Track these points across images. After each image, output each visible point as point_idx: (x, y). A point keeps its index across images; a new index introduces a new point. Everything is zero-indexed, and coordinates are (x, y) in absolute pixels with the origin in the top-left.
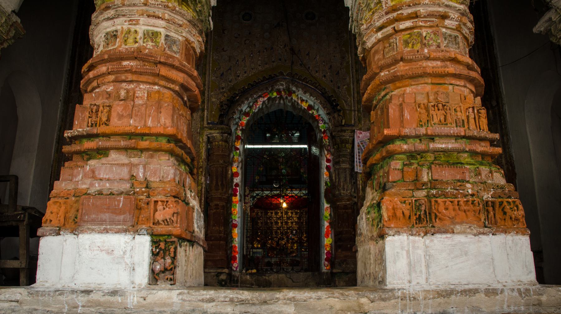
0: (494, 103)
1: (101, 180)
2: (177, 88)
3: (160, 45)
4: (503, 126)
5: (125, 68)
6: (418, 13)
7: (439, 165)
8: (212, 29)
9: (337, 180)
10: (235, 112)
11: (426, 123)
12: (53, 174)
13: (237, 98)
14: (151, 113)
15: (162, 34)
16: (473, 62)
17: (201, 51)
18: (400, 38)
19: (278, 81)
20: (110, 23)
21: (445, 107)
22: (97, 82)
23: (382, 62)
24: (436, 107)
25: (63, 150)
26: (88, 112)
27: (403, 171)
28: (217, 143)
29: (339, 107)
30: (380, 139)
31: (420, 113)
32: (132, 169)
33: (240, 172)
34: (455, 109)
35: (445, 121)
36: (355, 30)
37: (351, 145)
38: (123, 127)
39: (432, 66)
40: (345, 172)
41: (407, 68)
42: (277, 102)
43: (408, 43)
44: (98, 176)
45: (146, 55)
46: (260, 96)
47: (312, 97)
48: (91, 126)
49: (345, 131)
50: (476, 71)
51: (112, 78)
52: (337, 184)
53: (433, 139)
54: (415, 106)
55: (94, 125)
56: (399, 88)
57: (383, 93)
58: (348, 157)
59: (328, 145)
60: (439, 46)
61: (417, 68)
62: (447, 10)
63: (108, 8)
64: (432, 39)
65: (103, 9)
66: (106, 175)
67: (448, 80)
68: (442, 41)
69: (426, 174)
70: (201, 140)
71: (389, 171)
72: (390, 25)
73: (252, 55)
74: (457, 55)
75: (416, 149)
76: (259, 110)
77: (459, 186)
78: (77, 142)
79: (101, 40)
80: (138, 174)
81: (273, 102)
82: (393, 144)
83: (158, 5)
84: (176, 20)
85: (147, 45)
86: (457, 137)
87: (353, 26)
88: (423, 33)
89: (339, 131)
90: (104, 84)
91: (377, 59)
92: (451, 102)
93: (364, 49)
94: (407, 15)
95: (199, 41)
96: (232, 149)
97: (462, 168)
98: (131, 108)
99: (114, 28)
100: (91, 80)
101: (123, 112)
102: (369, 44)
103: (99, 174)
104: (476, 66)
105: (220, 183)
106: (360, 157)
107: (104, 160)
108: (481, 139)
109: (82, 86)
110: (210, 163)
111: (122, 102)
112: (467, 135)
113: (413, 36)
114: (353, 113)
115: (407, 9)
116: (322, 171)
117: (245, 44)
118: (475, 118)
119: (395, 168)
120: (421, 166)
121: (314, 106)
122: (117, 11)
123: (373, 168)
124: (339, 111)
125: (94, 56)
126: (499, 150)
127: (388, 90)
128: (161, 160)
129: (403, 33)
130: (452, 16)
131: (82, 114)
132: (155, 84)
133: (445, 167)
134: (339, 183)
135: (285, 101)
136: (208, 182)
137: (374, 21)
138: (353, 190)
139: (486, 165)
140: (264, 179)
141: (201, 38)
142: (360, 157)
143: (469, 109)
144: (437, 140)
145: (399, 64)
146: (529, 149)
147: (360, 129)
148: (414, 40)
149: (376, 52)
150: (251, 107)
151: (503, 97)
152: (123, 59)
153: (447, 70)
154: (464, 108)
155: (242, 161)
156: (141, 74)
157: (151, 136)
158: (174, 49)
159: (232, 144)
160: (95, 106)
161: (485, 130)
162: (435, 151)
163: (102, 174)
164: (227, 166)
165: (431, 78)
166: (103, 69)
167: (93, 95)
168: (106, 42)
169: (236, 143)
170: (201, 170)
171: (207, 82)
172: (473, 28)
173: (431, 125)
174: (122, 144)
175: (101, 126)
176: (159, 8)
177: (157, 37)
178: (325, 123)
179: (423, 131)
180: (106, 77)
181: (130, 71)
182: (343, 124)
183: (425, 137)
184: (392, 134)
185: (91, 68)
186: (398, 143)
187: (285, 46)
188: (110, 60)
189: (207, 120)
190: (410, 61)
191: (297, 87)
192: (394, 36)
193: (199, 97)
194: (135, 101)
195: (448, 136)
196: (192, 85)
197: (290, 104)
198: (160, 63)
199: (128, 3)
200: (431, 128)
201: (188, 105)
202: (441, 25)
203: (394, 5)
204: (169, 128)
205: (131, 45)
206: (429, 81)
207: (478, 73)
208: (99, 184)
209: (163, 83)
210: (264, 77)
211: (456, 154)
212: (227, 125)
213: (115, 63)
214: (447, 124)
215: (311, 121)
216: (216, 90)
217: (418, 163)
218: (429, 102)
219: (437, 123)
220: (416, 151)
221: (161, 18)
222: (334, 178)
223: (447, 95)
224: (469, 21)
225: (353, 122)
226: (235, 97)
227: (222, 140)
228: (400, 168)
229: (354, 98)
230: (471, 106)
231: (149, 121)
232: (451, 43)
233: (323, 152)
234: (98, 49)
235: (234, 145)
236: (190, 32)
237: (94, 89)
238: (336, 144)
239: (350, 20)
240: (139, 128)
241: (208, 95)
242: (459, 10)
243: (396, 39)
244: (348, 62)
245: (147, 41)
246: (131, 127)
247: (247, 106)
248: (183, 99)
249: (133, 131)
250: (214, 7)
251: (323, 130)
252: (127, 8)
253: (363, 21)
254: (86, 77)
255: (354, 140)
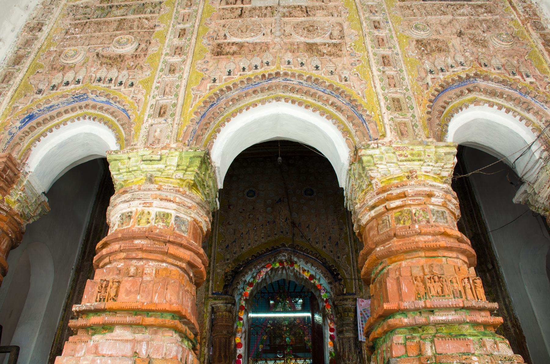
0: (490, 266)
1: (103, 356)
2: (184, 265)
3: (170, 225)
4: (503, 288)
5: (136, 246)
6: (406, 193)
7: (442, 337)
8: (218, 209)
9: (342, 350)
10: (239, 283)
11: (424, 296)
12: (55, 342)
13: (241, 269)
14: (157, 289)
15: (173, 215)
16: (462, 234)
17: (208, 230)
18: (391, 215)
19: (280, 252)
20: (126, 205)
21: (441, 279)
22: (109, 259)
23: (377, 238)
24: (432, 280)
25: (69, 324)
26: (98, 287)
27: (405, 346)
28: (221, 313)
29: (339, 276)
30: (381, 313)
31: (417, 286)
32: (135, 346)
33: (243, 342)
34: (450, 281)
35: (442, 293)
36: (350, 207)
37: (354, 314)
38: (130, 303)
39: (424, 240)
40: (349, 342)
41: (401, 243)
42: (280, 272)
43: (400, 220)
44: (101, 352)
45: (157, 234)
46: (264, 267)
47: (313, 267)
48: (100, 301)
49: (346, 300)
50: (466, 243)
51: (123, 255)
52: (341, 354)
53: (432, 311)
54: (412, 279)
55: (102, 300)
56: (395, 262)
57: (380, 267)
58: (352, 326)
59: (331, 314)
60: (428, 222)
61: (411, 243)
62: (432, 189)
63: (125, 192)
64: (421, 215)
65: (121, 193)
66: (109, 351)
67: (441, 253)
68: (430, 217)
69: (429, 347)
70: (205, 310)
71: (391, 346)
72: (381, 204)
73: (255, 229)
74: (446, 229)
75: (417, 323)
76: (262, 280)
77: (464, 360)
78: (84, 316)
79: (117, 220)
80: (141, 350)
81: (275, 272)
82: (394, 318)
83: (170, 190)
84: (186, 203)
85: (158, 225)
86: (457, 309)
87: (348, 204)
88: (412, 210)
89: (341, 300)
90: (115, 261)
91: (372, 236)
92: (445, 273)
93: (359, 226)
94: (396, 195)
95: (206, 221)
96: (235, 319)
97: (466, 340)
98: (139, 284)
99: (129, 210)
100: (104, 256)
101: (131, 288)
102: (364, 221)
103: (102, 350)
104: (465, 238)
105: (222, 355)
106: (364, 326)
107: (108, 335)
108: (481, 309)
109: (95, 262)
110: (214, 334)
111: (131, 278)
112: (466, 306)
113: (404, 213)
114: (354, 281)
115: (396, 189)
116: (326, 340)
117: (249, 218)
118: (471, 288)
119: (397, 342)
120: (423, 339)
121: (316, 275)
122: (133, 195)
123: (376, 342)
124: (340, 280)
125: (109, 234)
126: (500, 319)
127: (384, 265)
128: (164, 336)
129: (394, 211)
130: (437, 194)
131: (92, 289)
132: (163, 261)
133: (448, 339)
134: (343, 354)
135: (287, 271)
136: (211, 353)
137: (367, 201)
138: (359, 360)
139: (489, 336)
140: (268, 348)
141: (208, 219)
142: (364, 326)
143: (464, 280)
144: (437, 312)
145: (393, 240)
146: (533, 311)
147: (362, 297)
148: (405, 217)
149: (371, 229)
150: (254, 278)
151: (498, 260)
152: (135, 238)
153: (439, 243)
154: (459, 279)
155: (245, 332)
156: (150, 252)
157: (157, 312)
158: (182, 229)
159: (236, 314)
160: (105, 282)
161: (483, 300)
162: (437, 324)
163: (105, 350)
164: (230, 337)
165: (425, 252)
166: (116, 246)
167: (105, 271)
168: (121, 222)
169: (240, 313)
170: (204, 340)
171: (212, 253)
172: (458, 204)
173: (430, 298)
174: (128, 320)
175: (109, 301)
176: (170, 192)
177: (167, 218)
178: (327, 292)
179: (421, 304)
180: (118, 254)
181: (141, 250)
182: (345, 292)
183: (424, 310)
184: (392, 308)
185: (105, 245)
186: (398, 317)
187: (286, 219)
188: (123, 239)
189: (212, 290)
190: (403, 237)
191: (298, 258)
192: (386, 214)
193: (205, 273)
194: (144, 277)
195: (447, 309)
196: (198, 262)
197: (292, 274)
198: (169, 242)
199: (144, 188)
200: (429, 300)
201: (193, 281)
202: (428, 202)
203: (383, 186)
204: (174, 305)
205: (144, 225)
206: (423, 254)
207: (468, 244)
208: (101, 360)
209: (171, 260)
210: (267, 249)
211: (457, 326)
212: (231, 296)
213: (127, 242)
214: (444, 296)
215: (313, 291)
216: (221, 261)
217: (420, 337)
218: (425, 275)
219: (435, 295)
220: (417, 324)
221: (172, 201)
222: (338, 348)
223: (441, 267)
224: (454, 198)
225: (354, 290)
226: (239, 268)
227: (226, 311)
228: (403, 342)
229: (354, 267)
230: (466, 276)
231: (155, 297)
232: (439, 218)
233: (326, 321)
234: (113, 228)
235: (238, 315)
236: (198, 213)
237: (105, 264)
238: (339, 313)
239: (345, 199)
240: (145, 304)
241: (214, 266)
242: (443, 188)
243: (388, 217)
244: (346, 233)
245: (158, 222)
246: (137, 303)
247: (250, 276)
248: (189, 275)
249: (139, 307)
250: (220, 190)
251: (325, 299)
252: (142, 193)
253: (357, 201)
254: (99, 254)
255: (356, 308)
